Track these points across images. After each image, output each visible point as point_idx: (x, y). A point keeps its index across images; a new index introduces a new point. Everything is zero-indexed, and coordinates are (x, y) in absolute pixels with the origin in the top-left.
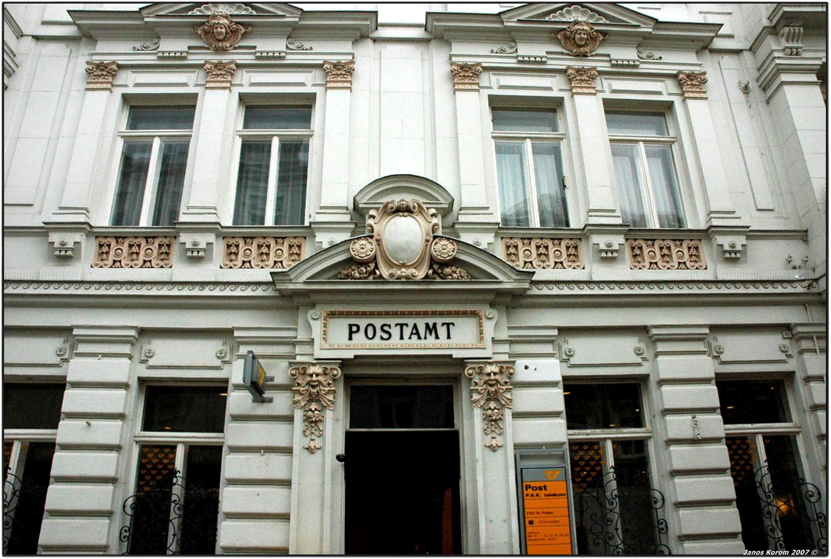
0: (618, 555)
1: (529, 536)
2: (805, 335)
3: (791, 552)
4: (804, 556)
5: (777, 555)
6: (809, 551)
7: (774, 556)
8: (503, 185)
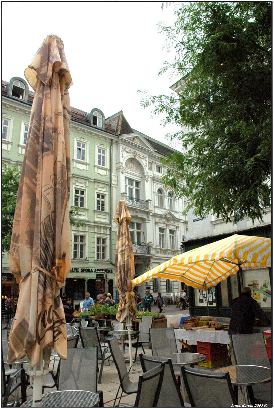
3: (254, 406)
4: (261, 407)
7: (246, 407)
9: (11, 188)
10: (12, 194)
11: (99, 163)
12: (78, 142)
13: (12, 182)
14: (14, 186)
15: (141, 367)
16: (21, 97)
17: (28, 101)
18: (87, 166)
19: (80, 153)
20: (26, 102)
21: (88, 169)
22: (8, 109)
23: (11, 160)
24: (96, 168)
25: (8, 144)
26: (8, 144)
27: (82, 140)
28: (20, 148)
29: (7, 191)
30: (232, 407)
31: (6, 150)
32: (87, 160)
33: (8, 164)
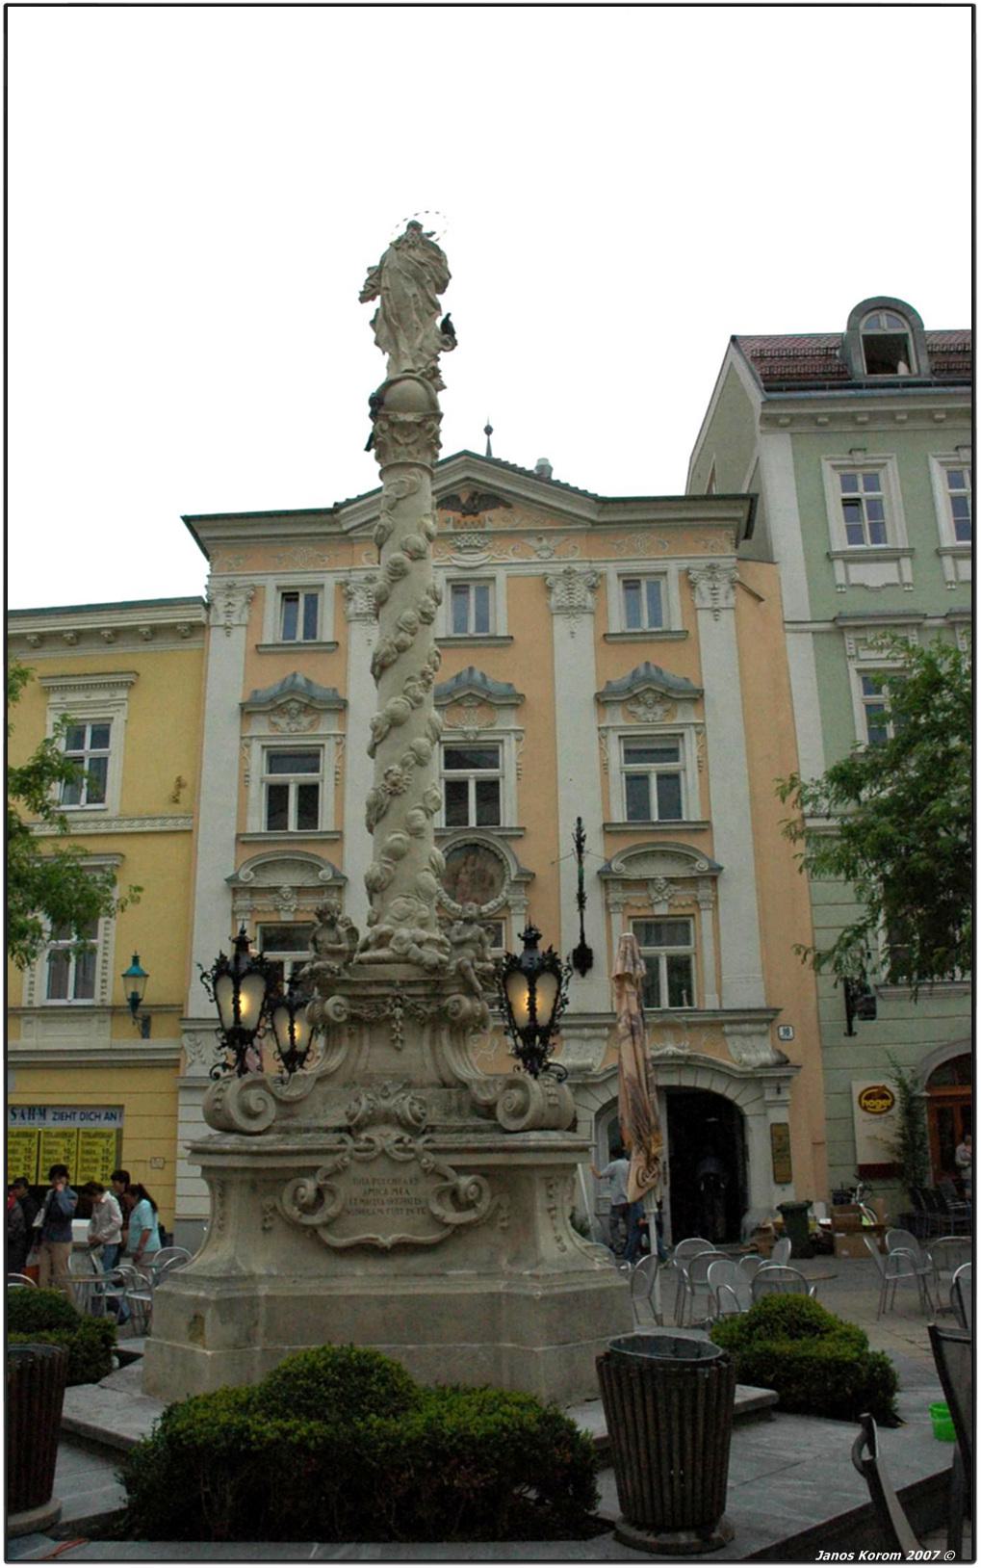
1: (45, 1152)
4: (930, 1562)
5: (880, 1561)
6: (939, 1552)
7: (874, 1562)
9: (946, 720)
10: (955, 742)
11: (855, 535)
12: (843, 472)
13: (947, 697)
14: (957, 712)
15: (941, 1388)
16: (902, 368)
17: (933, 372)
18: (906, 563)
19: (858, 517)
20: (929, 380)
21: (908, 578)
22: (907, 427)
23: (925, 617)
24: (839, 565)
25: (897, 559)
26: (897, 559)
27: (859, 458)
28: (948, 561)
29: (934, 737)
30: (822, 1562)
31: (896, 585)
32: (898, 536)
33: (915, 632)
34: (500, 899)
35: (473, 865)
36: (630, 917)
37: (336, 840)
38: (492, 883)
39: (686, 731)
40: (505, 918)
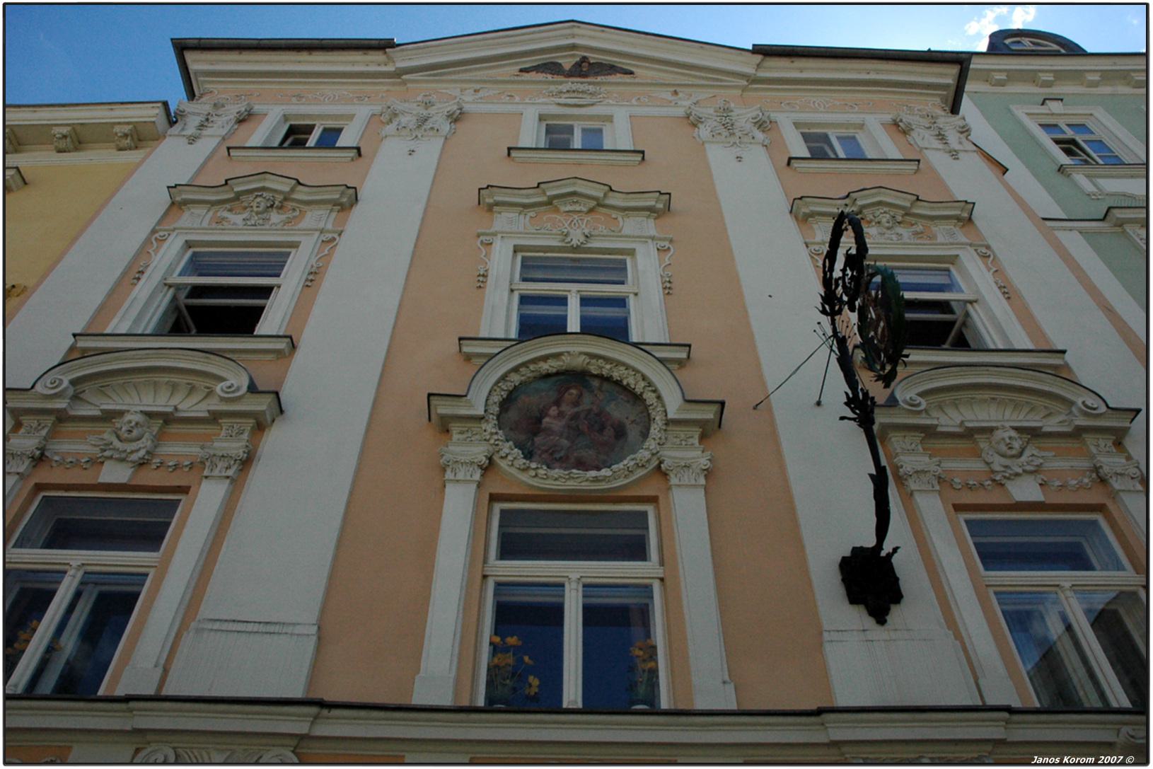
0: (165, 763)
2: (495, 725)
4: (1115, 764)
5: (1079, 764)
7: (1074, 764)
8: (477, 636)
30: (1036, 764)
34: (643, 454)
35: (576, 403)
36: (958, 508)
37: (278, 352)
38: (620, 432)
39: (640, 248)
40: (653, 500)
